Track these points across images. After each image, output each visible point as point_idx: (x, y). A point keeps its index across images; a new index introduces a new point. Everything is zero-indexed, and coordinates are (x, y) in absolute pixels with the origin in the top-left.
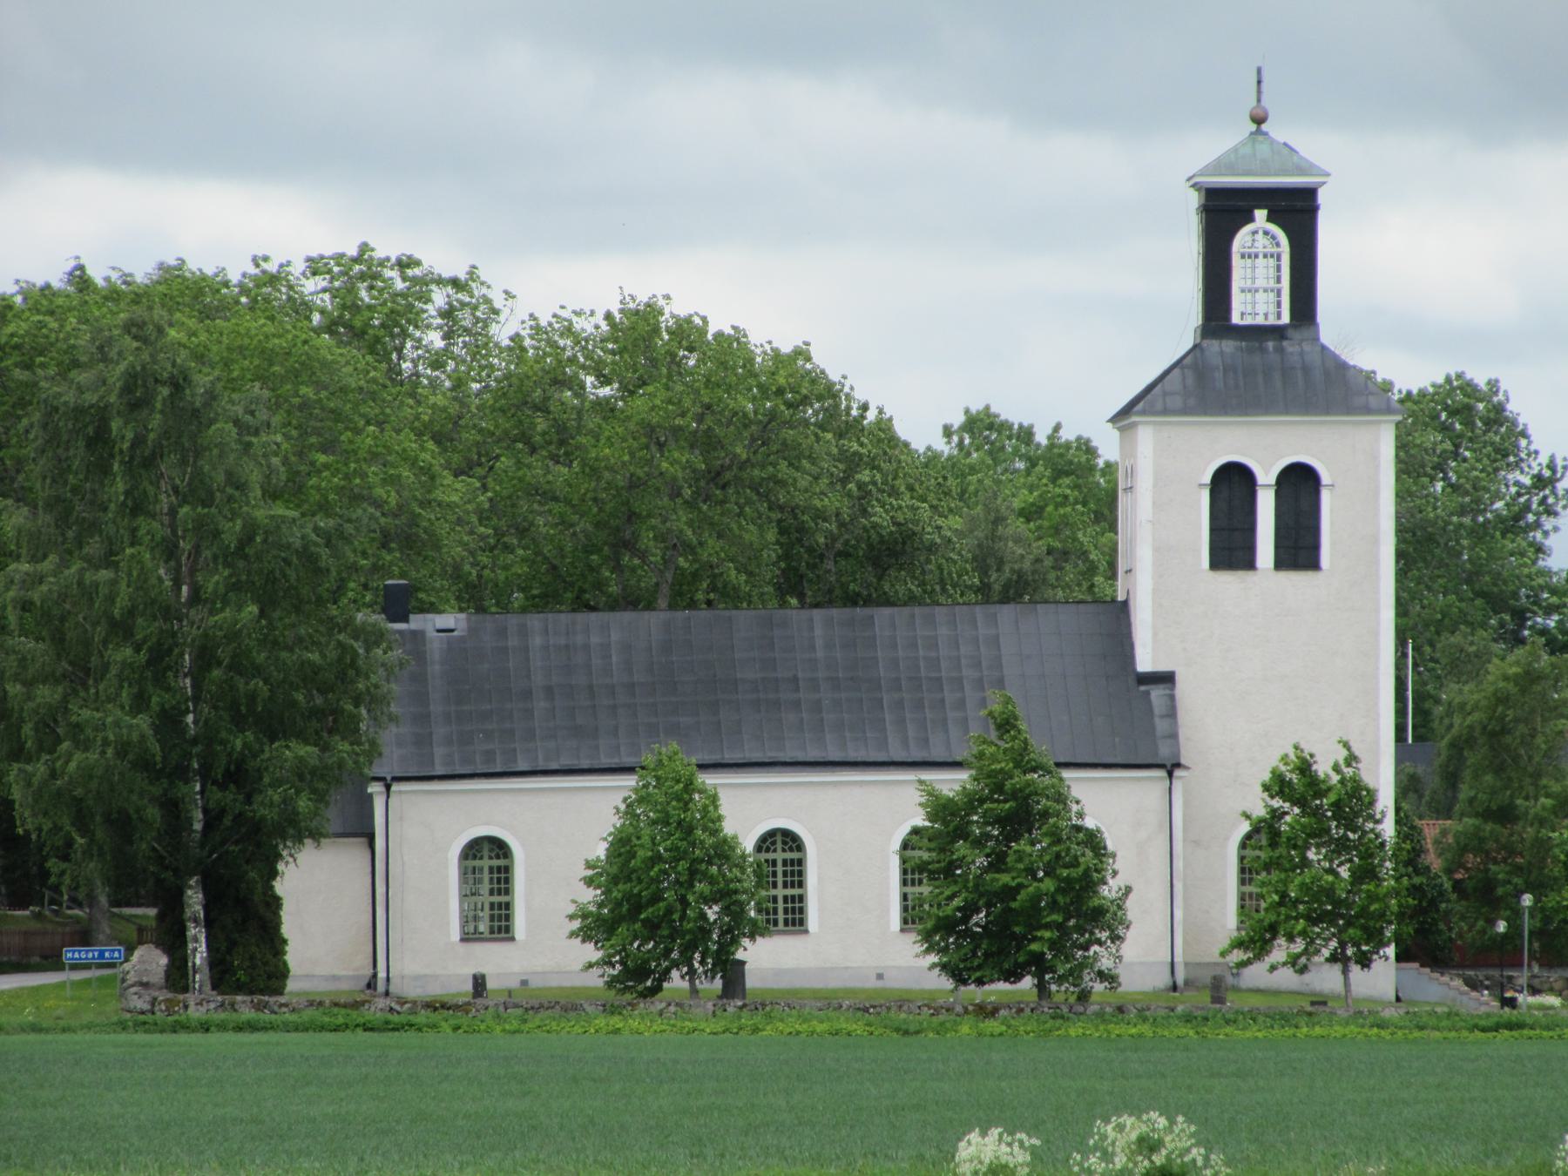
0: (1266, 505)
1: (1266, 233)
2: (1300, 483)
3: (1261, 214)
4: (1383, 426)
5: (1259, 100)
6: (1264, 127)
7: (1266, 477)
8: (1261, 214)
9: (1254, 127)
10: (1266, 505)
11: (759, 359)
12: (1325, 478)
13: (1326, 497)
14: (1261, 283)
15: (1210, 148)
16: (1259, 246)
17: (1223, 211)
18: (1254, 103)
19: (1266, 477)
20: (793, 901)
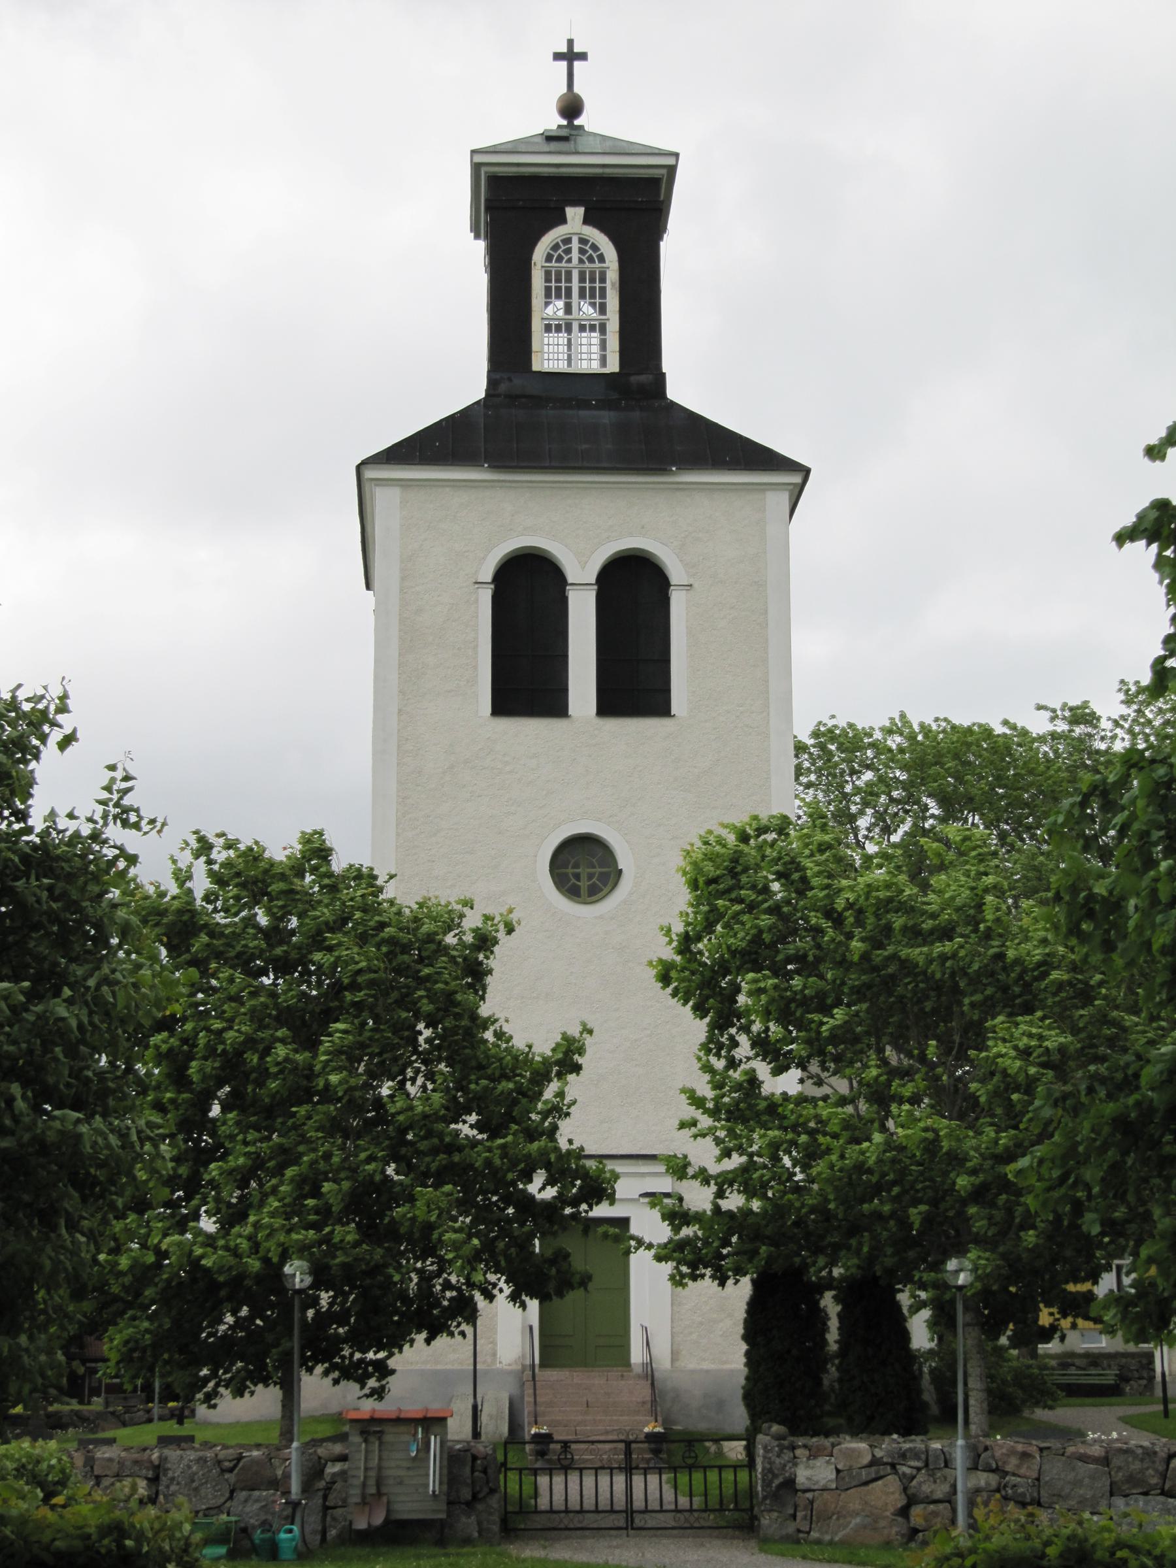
1: (583, 241)
3: (575, 214)
6: (576, 122)
7: (581, 570)
8: (575, 214)
12: (676, 573)
15: (520, 116)
18: (564, 90)
19: (581, 570)
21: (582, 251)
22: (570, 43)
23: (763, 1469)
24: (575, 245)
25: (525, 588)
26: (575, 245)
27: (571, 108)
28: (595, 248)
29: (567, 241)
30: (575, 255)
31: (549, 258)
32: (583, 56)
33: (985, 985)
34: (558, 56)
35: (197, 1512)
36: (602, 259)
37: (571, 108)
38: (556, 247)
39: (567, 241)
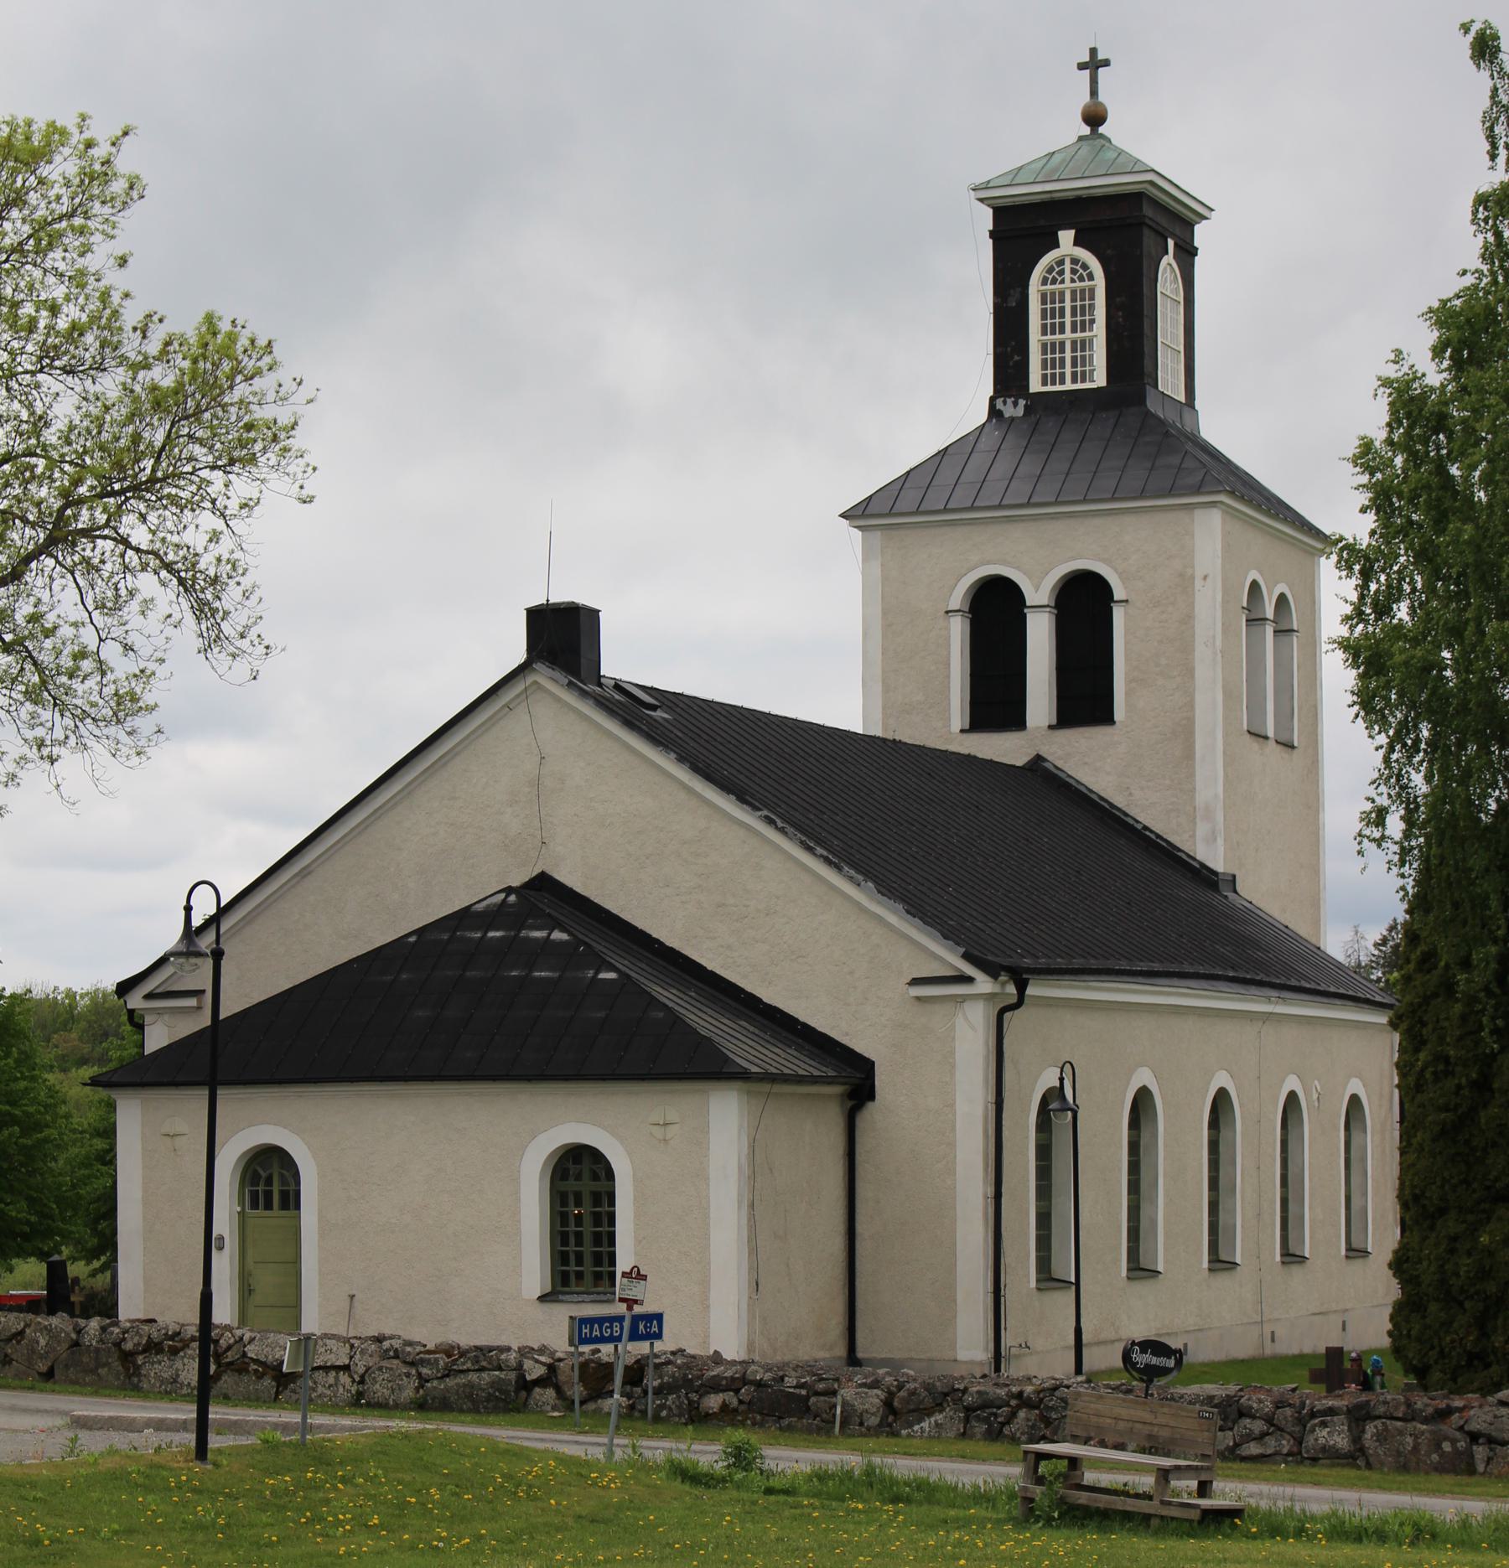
0: (1040, 634)
1: (1075, 261)
2: (1085, 603)
3: (1066, 237)
4: (1199, 514)
5: (1094, 92)
6: (1101, 130)
7: (1038, 592)
8: (1066, 237)
9: (1086, 130)
10: (1040, 634)
11: (1357, 567)
12: (1119, 593)
13: (1119, 615)
14: (331, 1380)
15: (1031, 140)
16: (1070, 265)
17: (1021, 230)
18: (1086, 98)
19: (1038, 592)
20: (1053, 375)
21: (1074, 271)
22: (1093, 51)
23: (653, 1001)
24: (1067, 266)
25: (995, 609)
26: (1067, 266)
27: (1094, 118)
28: (1085, 267)
29: (1061, 262)
30: (1067, 275)
31: (1044, 282)
32: (1106, 63)
33: (38, 504)
34: (1082, 66)
35: (234, 656)
36: (1091, 277)
37: (1094, 118)
38: (1050, 270)
39: (1061, 262)
